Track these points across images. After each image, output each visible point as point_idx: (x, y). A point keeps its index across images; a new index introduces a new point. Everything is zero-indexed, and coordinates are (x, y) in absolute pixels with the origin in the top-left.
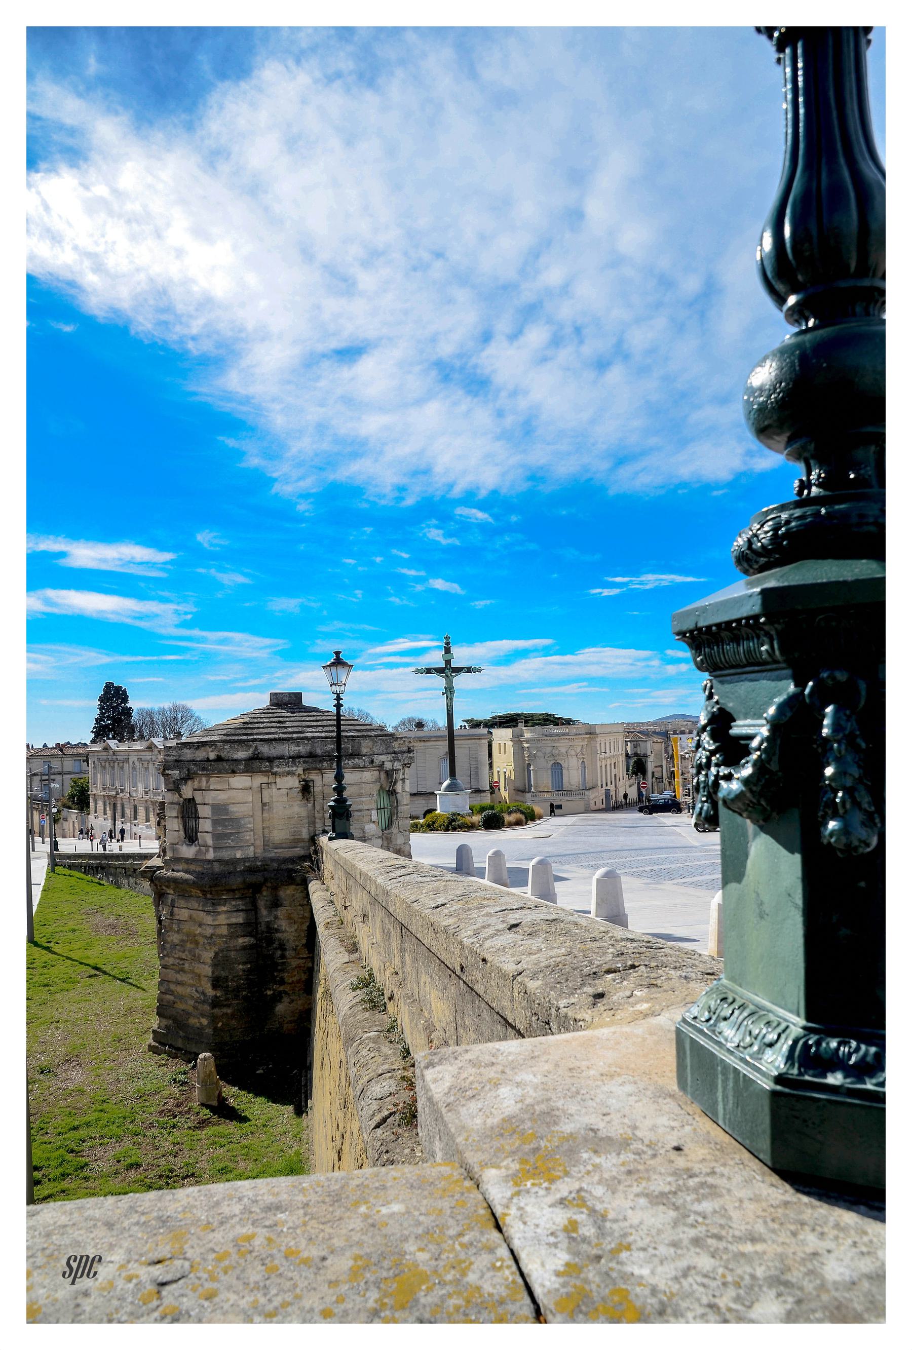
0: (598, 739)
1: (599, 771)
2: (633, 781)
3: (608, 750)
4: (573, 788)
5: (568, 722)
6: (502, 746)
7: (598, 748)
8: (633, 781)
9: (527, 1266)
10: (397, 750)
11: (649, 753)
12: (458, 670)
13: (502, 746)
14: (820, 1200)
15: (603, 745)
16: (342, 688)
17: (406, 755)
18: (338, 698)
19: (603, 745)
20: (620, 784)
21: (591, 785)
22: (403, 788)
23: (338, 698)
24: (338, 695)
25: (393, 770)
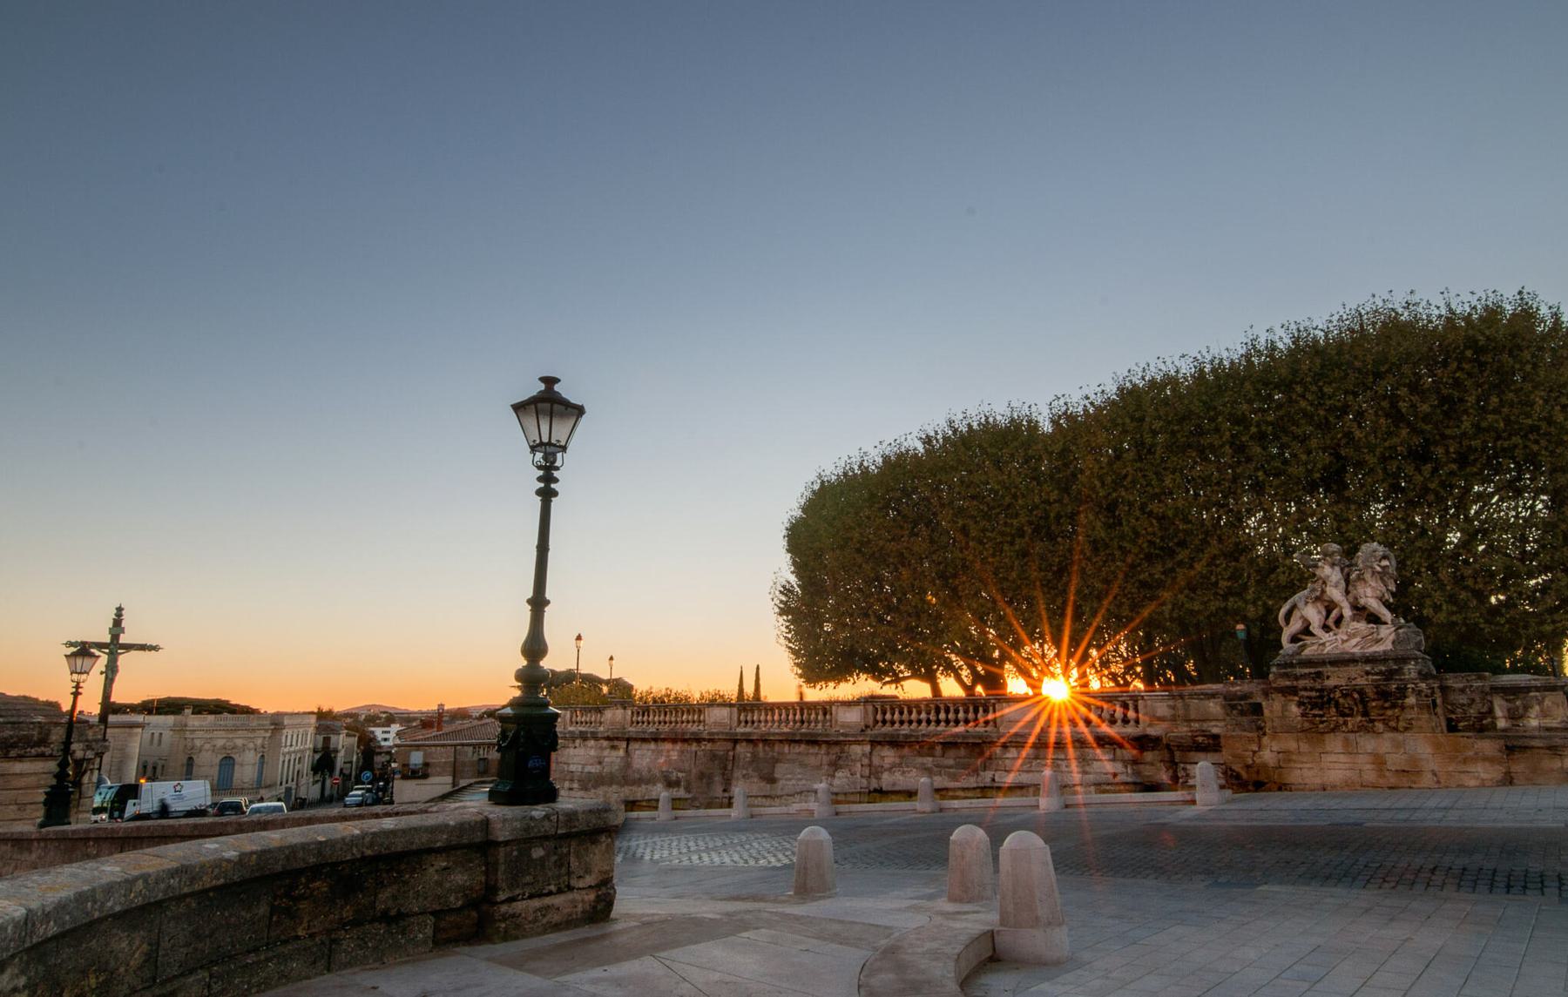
0: (285, 731)
1: (280, 766)
2: (318, 777)
3: (294, 743)
4: (246, 786)
5: (247, 711)
6: (156, 736)
7: (284, 741)
8: (318, 777)
9: (422, 843)
10: (90, 738)
11: (340, 747)
12: (128, 647)
13: (156, 736)
14: (470, 944)
15: (289, 737)
16: (84, 676)
17: (101, 744)
18: (78, 687)
19: (289, 737)
20: (303, 781)
21: (269, 783)
22: (90, 779)
23: (78, 687)
24: (78, 683)
25: (84, 759)
